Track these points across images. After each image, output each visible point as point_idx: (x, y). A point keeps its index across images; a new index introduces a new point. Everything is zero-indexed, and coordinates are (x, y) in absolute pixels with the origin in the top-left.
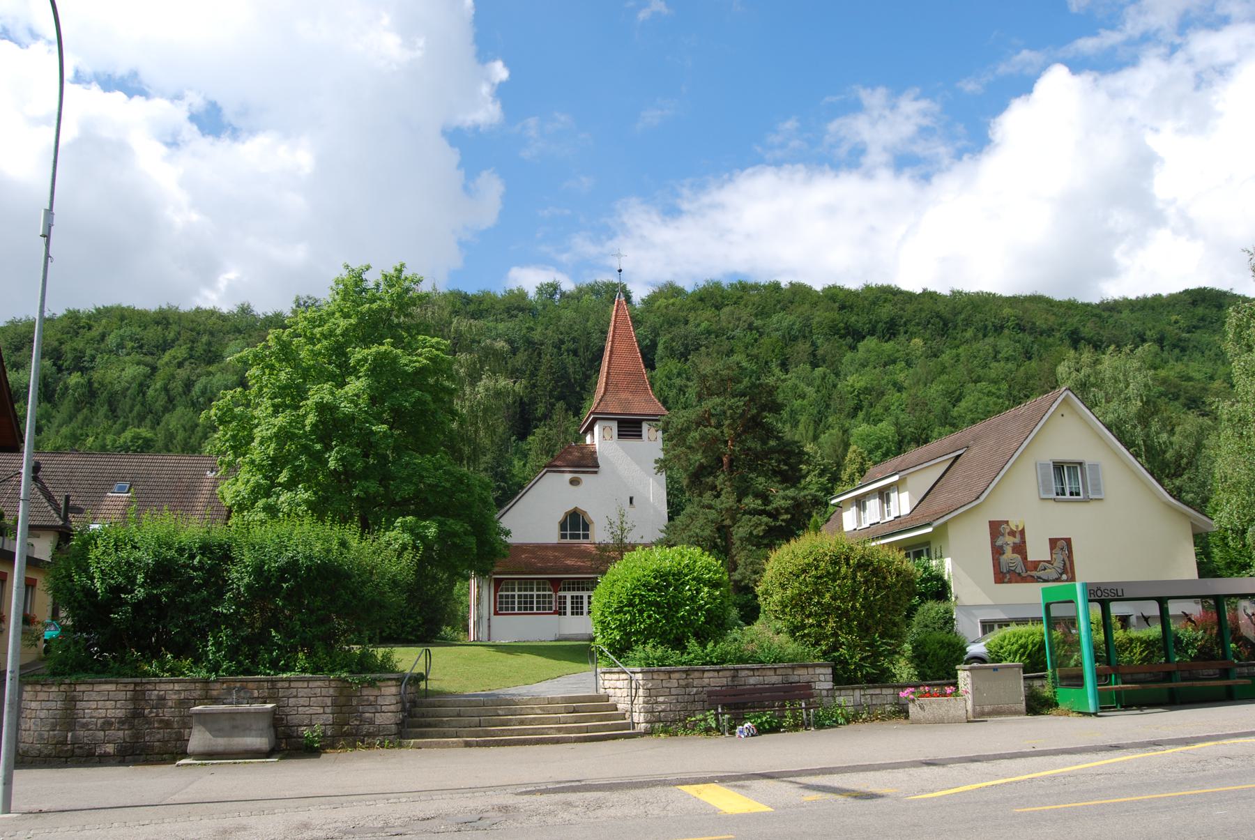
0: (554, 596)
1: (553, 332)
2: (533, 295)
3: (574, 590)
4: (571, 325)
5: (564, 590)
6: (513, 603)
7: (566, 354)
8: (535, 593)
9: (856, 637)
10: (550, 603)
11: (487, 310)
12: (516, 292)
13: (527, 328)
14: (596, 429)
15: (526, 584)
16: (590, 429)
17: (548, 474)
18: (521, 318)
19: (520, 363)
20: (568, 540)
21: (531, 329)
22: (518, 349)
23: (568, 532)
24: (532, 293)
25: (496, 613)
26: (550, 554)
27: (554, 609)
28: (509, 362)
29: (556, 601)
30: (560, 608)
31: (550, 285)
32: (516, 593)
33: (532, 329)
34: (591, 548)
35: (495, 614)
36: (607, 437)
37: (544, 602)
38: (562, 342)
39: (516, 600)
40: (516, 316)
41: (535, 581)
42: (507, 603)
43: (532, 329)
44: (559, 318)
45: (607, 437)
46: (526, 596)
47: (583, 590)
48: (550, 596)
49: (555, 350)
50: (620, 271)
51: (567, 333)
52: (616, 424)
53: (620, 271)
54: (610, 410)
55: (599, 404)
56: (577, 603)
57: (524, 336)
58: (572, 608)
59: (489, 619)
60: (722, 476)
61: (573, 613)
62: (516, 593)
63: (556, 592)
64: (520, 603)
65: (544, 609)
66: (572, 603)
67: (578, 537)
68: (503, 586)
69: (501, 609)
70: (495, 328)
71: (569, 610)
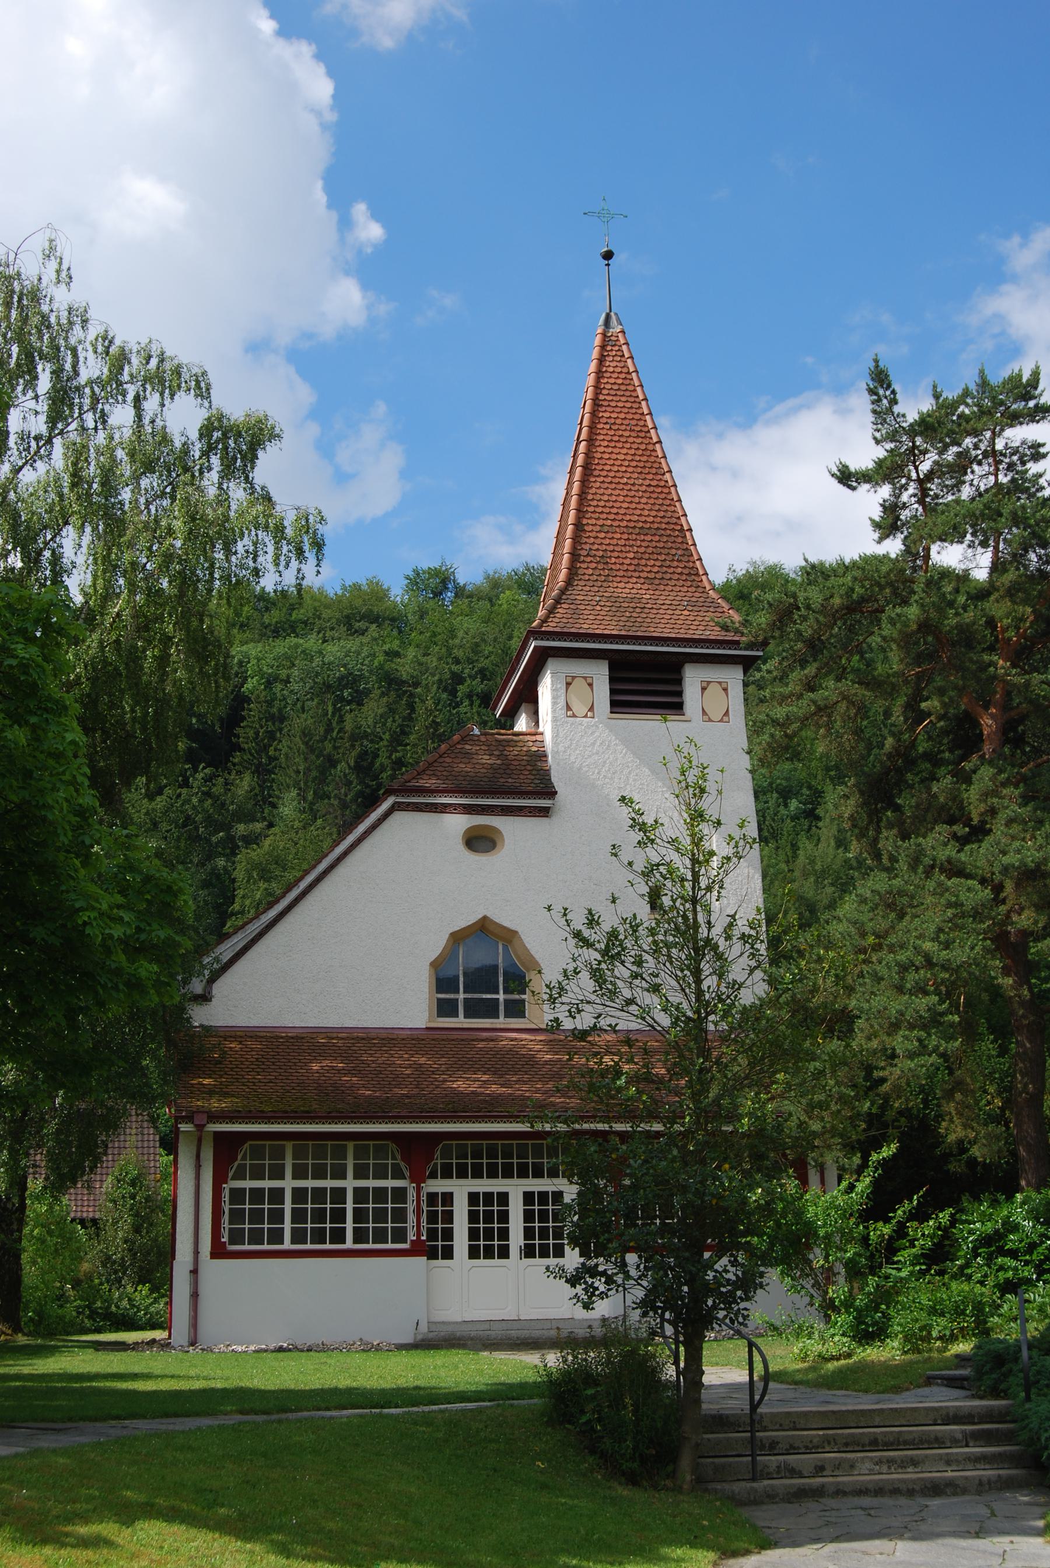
0: (411, 1194)
1: (440, 659)
2: (400, 592)
3: (477, 1174)
4: (477, 645)
5: (447, 1174)
6: (277, 1216)
7: (466, 703)
8: (350, 1184)
9: (899, 1266)
10: (400, 1215)
11: (305, 623)
12: (365, 588)
13: (387, 653)
14: (546, 690)
15: (320, 1154)
16: (527, 696)
17: (398, 817)
18: (375, 635)
19: (370, 721)
20: (461, 1021)
21: (392, 655)
22: (367, 692)
23: (461, 996)
24: (397, 592)
25: (219, 1252)
26: (402, 1061)
27: (411, 1236)
28: (348, 718)
29: (418, 1212)
30: (432, 1234)
31: (435, 573)
32: (288, 1184)
33: (397, 654)
34: (534, 1043)
35: (214, 1255)
36: (580, 709)
37: (380, 1215)
38: (458, 679)
39: (288, 1206)
40: (363, 632)
41: (350, 1146)
42: (257, 1216)
43: (397, 654)
44: (452, 633)
45: (580, 709)
46: (319, 1194)
47: (508, 1174)
48: (400, 1195)
49: (444, 696)
50: (608, 255)
51: (470, 661)
52: (605, 670)
53: (608, 255)
54: (585, 628)
55: (551, 611)
56: (489, 1217)
57: (381, 667)
58: (473, 1234)
59: (195, 1272)
60: (986, 773)
61: (474, 1253)
62: (288, 1184)
63: (418, 1179)
64: (298, 1216)
65: (380, 1236)
66: (473, 1217)
67: (490, 1010)
68: (243, 1158)
69: (236, 1237)
70: (320, 652)
71: (461, 1241)
